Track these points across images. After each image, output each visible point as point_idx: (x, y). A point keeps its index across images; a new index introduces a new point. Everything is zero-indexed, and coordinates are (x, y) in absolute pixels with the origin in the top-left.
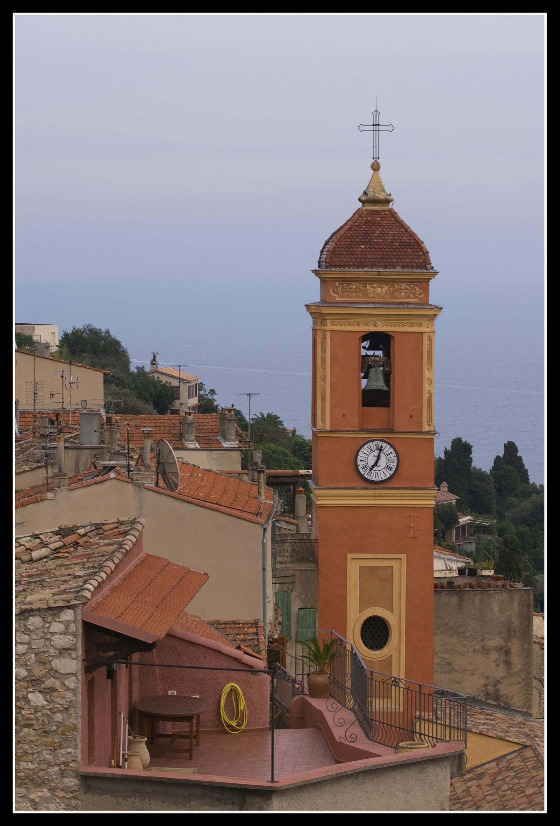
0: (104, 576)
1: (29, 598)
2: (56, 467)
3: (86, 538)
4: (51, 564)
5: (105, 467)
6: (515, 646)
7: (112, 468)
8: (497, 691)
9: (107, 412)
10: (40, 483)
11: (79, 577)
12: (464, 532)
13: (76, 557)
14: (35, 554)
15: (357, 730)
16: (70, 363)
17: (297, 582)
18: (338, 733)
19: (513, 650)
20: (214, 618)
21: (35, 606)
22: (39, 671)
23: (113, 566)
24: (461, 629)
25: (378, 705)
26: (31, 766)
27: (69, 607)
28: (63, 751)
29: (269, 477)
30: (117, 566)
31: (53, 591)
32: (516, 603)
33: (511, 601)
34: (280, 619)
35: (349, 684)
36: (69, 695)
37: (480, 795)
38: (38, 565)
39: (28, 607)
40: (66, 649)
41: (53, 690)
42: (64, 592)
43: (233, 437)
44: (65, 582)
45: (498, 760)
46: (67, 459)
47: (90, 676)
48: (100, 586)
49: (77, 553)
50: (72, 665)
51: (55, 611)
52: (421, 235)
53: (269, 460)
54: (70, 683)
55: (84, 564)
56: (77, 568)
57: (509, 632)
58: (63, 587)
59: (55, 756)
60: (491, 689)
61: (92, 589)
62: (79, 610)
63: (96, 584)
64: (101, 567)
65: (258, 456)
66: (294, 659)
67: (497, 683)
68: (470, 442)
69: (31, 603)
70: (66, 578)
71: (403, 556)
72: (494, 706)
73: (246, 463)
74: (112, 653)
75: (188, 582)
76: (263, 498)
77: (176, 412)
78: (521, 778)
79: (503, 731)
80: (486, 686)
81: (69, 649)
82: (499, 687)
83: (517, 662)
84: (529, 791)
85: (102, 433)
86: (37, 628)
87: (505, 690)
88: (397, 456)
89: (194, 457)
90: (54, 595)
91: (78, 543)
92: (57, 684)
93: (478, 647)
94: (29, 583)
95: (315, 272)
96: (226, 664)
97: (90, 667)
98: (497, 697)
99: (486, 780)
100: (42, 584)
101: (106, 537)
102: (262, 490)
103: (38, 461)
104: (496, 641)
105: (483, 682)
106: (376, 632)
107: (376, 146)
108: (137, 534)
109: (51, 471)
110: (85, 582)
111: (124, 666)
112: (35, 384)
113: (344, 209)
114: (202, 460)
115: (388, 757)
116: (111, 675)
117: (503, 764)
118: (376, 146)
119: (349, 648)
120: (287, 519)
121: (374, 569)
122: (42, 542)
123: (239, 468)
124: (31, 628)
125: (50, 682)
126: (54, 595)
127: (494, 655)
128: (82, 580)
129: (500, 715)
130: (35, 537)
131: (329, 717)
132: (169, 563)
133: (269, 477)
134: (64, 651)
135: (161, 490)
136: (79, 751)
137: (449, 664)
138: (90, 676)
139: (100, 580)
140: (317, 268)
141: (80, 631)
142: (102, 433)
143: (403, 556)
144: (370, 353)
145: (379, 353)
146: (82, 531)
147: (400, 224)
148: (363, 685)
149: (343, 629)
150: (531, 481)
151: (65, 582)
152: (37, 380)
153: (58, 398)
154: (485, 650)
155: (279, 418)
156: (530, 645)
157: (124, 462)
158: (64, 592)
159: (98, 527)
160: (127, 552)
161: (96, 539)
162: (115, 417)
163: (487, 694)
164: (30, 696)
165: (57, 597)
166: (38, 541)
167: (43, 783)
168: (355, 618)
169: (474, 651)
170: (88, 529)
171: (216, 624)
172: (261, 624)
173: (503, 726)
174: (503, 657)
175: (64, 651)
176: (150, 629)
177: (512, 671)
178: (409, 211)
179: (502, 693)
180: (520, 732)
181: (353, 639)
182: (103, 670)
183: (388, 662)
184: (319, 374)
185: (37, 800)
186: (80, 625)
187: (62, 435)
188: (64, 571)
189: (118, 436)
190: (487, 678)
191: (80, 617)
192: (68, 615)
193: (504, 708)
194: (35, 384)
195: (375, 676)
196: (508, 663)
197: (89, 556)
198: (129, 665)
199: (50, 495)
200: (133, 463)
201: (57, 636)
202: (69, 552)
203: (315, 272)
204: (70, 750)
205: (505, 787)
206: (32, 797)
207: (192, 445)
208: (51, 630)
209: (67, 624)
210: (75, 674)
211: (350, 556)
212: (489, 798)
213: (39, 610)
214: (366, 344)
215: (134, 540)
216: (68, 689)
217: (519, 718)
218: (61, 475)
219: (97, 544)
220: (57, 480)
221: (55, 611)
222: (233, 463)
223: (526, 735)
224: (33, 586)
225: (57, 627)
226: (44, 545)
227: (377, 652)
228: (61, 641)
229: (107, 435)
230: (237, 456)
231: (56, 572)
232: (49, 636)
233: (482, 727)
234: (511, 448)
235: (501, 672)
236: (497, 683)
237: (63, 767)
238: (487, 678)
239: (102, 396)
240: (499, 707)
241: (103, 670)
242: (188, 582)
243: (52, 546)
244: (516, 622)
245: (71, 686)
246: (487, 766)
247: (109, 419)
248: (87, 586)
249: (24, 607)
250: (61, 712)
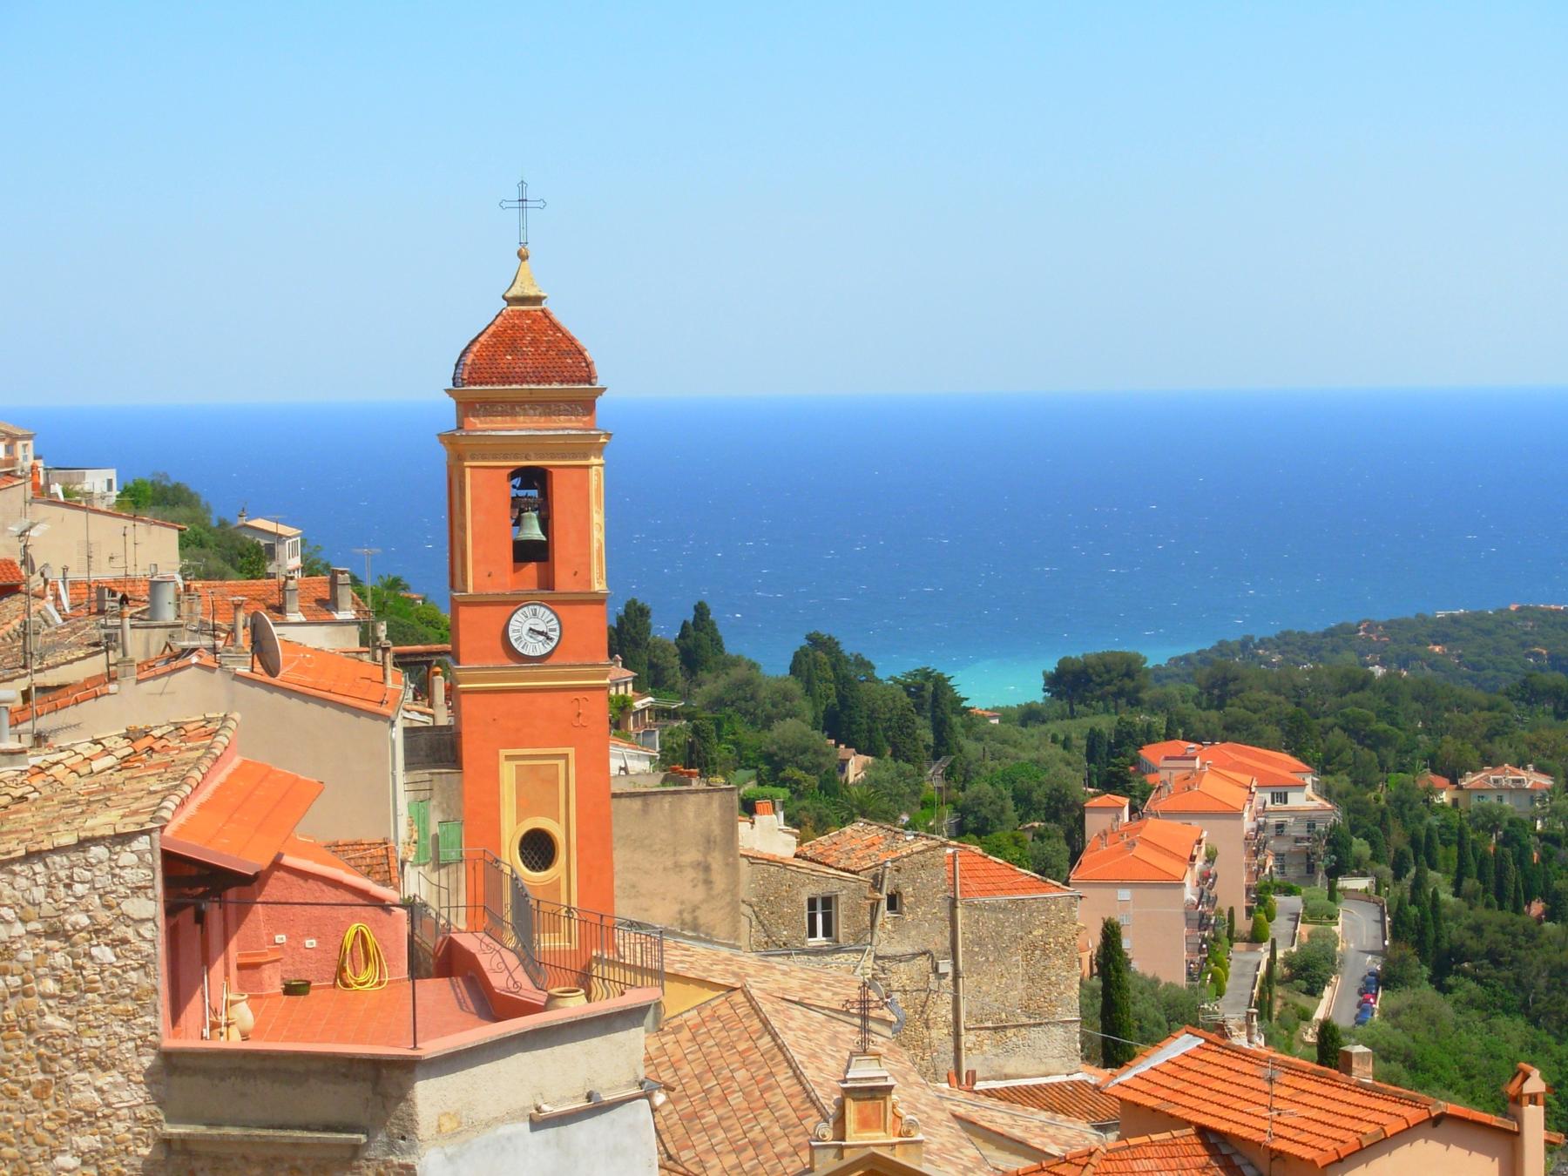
0: (188, 789)
1: (90, 823)
2: (120, 651)
3: (163, 742)
4: (118, 778)
5: (184, 650)
6: (716, 860)
7: (194, 650)
8: (695, 918)
9: (184, 579)
10: (99, 672)
11: (155, 792)
12: (643, 717)
13: (151, 767)
14: (97, 765)
15: (522, 977)
16: (134, 518)
17: (436, 788)
18: (498, 981)
19: (715, 866)
20: (331, 839)
21: (98, 833)
22: (104, 917)
23: (200, 777)
24: (647, 842)
25: (548, 942)
26: (96, 1043)
27: (143, 833)
28: (139, 1021)
29: (397, 655)
30: (204, 776)
31: (121, 812)
32: (715, 805)
33: (709, 804)
34: (415, 837)
35: (509, 918)
36: (146, 947)
37: (679, 1055)
38: (101, 778)
39: (89, 834)
40: (139, 888)
41: (124, 941)
42: (136, 813)
43: (349, 606)
44: (137, 799)
45: (699, 1008)
46: (138, 643)
47: (173, 921)
48: (182, 804)
49: (152, 762)
50: (150, 907)
51: (123, 839)
52: (582, 340)
53: (396, 635)
54: (147, 930)
55: (160, 775)
56: (153, 780)
57: (709, 842)
58: (134, 806)
59: (130, 1028)
60: (687, 917)
61: (173, 807)
62: (156, 835)
63: (178, 801)
64: (184, 779)
65: (382, 630)
66: (435, 889)
67: (695, 909)
68: (649, 604)
69: (93, 829)
70: (139, 794)
71: (571, 751)
72: (691, 938)
73: (368, 638)
74: (201, 890)
75: (296, 797)
76: (390, 683)
77: (271, 576)
78: (731, 1029)
79: (705, 970)
80: (681, 912)
81: (146, 888)
82: (697, 913)
83: (720, 881)
84: (742, 1046)
85: (178, 606)
86: (101, 862)
87: (705, 917)
88: (560, 623)
89: (300, 635)
90: (123, 816)
91: (151, 749)
92: (130, 933)
93: (669, 864)
94: (89, 803)
95: (448, 391)
96: (349, 898)
97: (171, 910)
98: (695, 927)
99: (685, 1034)
100: (106, 804)
101: (190, 739)
102: (389, 672)
103: (96, 644)
104: (691, 855)
105: (677, 907)
106: (538, 849)
107: (523, 227)
108: (229, 734)
109: (114, 657)
110: (164, 799)
111: (216, 905)
112: (89, 544)
113: (480, 312)
114: (317, 638)
115: (575, 1006)
116: (200, 918)
117: (706, 1013)
118: (523, 227)
119: (507, 870)
120: (421, 708)
121: (533, 768)
122: (105, 748)
123: (356, 646)
124: (93, 861)
125: (120, 931)
126: (123, 816)
127: (690, 874)
128: (159, 796)
129: (700, 948)
130: (96, 742)
131: (485, 961)
132: (271, 771)
133: (397, 655)
134: (137, 890)
135: (258, 677)
136: (160, 1020)
137: (633, 887)
138: (173, 921)
139: (183, 795)
140: (451, 386)
141: (159, 862)
142: (178, 606)
143: (571, 751)
144: (522, 493)
145: (534, 493)
146: (157, 733)
147: (557, 328)
148: (527, 917)
149: (498, 845)
150: (727, 651)
151: (137, 799)
152: (91, 539)
153: (119, 562)
154: (678, 867)
155: (1252, 638)
156: (735, 859)
157: (206, 641)
158: (136, 813)
159: (178, 727)
160: (217, 758)
161: (175, 743)
162: (198, 584)
163: (683, 924)
164: (94, 951)
165: (126, 820)
166: (100, 747)
167: (114, 1065)
168: (511, 832)
169: (665, 869)
170: (165, 730)
171: (335, 848)
172: (392, 844)
173: (705, 963)
174: (701, 876)
175: (137, 890)
176: (249, 860)
177: (715, 892)
178: (571, 314)
179: (702, 921)
180: (727, 971)
181: (511, 856)
182: (190, 912)
183: (555, 886)
184: (456, 523)
185: (106, 1088)
186: (158, 855)
187: (126, 609)
188: (135, 785)
189: (199, 609)
190: (682, 903)
191: (157, 845)
192: (142, 843)
193: (705, 941)
194: (89, 544)
195: (543, 907)
196: (708, 883)
197: (167, 766)
198: (223, 905)
199: (113, 687)
200: (220, 643)
201: (128, 870)
202: (141, 761)
203: (448, 391)
204: (148, 1019)
205: (712, 1042)
206: (98, 1084)
207: (299, 617)
208: (121, 864)
209: (140, 855)
210: (153, 920)
211: (503, 752)
212: (690, 1057)
213: (103, 838)
214: (517, 482)
215: (226, 742)
216: (144, 939)
217: (725, 952)
218: (125, 661)
219: (179, 749)
220: (120, 669)
221: (123, 839)
222: (349, 640)
223: (735, 974)
224: (94, 806)
225: (127, 857)
226: (107, 752)
227: (542, 874)
228: (134, 876)
229: (184, 608)
230: (354, 631)
231: (1022, 755)
232: (117, 871)
233: (678, 966)
234: (701, 610)
235: (699, 894)
236: (695, 909)
237: (139, 1042)
238: (682, 903)
239: (177, 558)
240: (698, 939)
241: (190, 912)
242: (296, 797)
243: (120, 754)
244: (717, 830)
245: (148, 935)
246: (685, 1016)
247: (187, 588)
248: (165, 804)
249: (83, 834)
250: (134, 969)
